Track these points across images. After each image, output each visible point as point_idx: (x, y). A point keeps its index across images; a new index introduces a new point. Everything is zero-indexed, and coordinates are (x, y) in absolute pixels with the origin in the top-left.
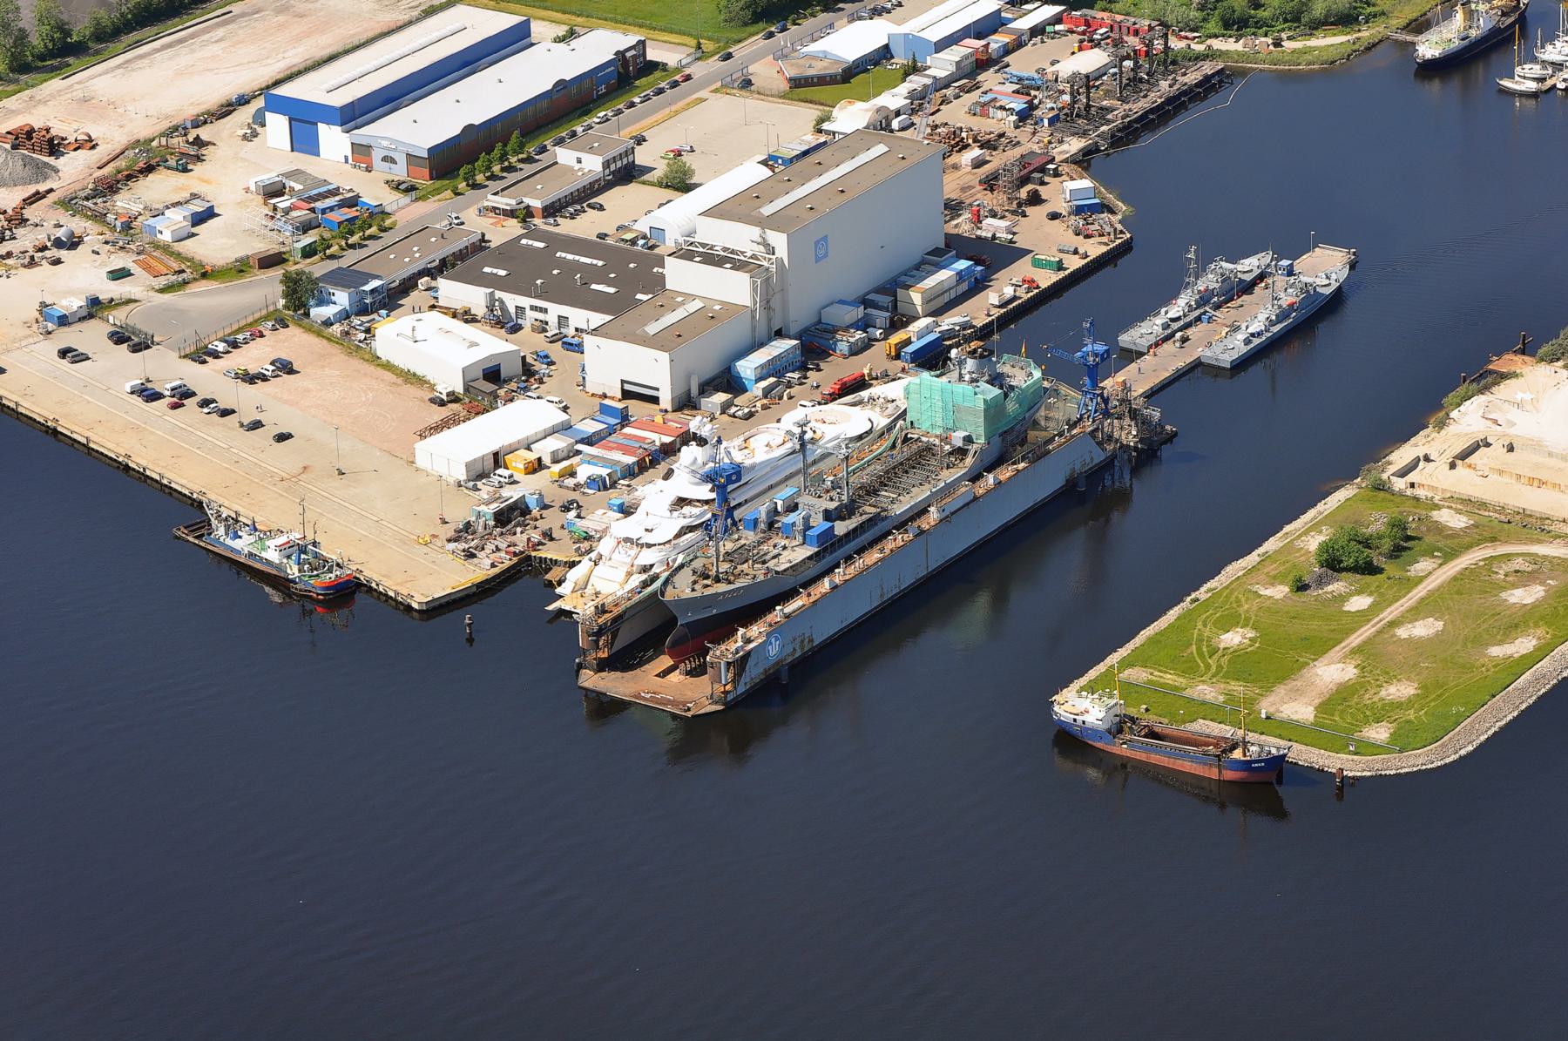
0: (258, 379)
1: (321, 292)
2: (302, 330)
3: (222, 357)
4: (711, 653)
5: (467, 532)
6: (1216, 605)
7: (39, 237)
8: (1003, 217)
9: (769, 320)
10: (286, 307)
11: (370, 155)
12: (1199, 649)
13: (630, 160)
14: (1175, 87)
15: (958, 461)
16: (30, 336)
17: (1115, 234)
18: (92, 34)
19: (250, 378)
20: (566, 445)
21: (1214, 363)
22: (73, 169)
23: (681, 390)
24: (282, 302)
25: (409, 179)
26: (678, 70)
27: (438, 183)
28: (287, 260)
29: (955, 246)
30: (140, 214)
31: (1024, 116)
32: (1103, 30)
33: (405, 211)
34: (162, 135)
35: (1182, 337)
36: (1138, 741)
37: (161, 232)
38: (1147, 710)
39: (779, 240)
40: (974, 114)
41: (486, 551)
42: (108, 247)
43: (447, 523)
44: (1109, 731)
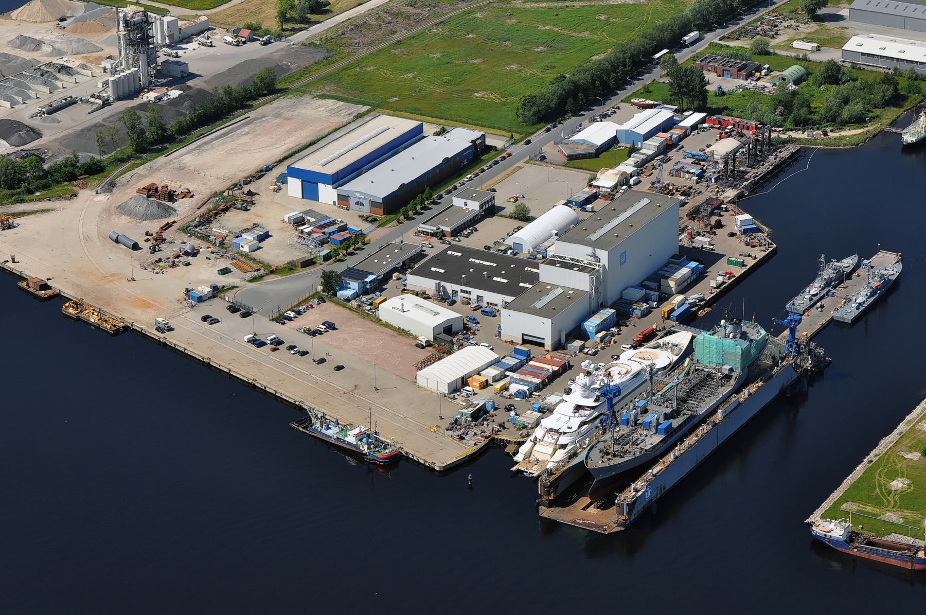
0: (317, 333)
1: (342, 282)
2: (334, 304)
3: (293, 320)
4: (618, 498)
5: (456, 425)
6: (883, 464)
7: (174, 249)
8: (704, 236)
9: (598, 298)
10: (323, 291)
11: (348, 201)
12: (881, 491)
13: (493, 203)
14: (778, 159)
15: (726, 382)
16: (183, 308)
17: (769, 245)
18: (177, 130)
19: (314, 333)
20: (499, 372)
21: (841, 320)
22: (183, 209)
23: (556, 339)
24: (320, 288)
25: (371, 214)
26: (503, 150)
27: (389, 217)
28: (316, 263)
29: (685, 254)
30: (227, 236)
31: (701, 176)
32: (730, 127)
33: (375, 234)
34: (229, 189)
35: (821, 305)
36: (863, 547)
37: (243, 247)
38: (862, 528)
39: (603, 255)
40: (672, 176)
41: (469, 435)
42: (214, 255)
43: (443, 419)
44: (846, 541)
